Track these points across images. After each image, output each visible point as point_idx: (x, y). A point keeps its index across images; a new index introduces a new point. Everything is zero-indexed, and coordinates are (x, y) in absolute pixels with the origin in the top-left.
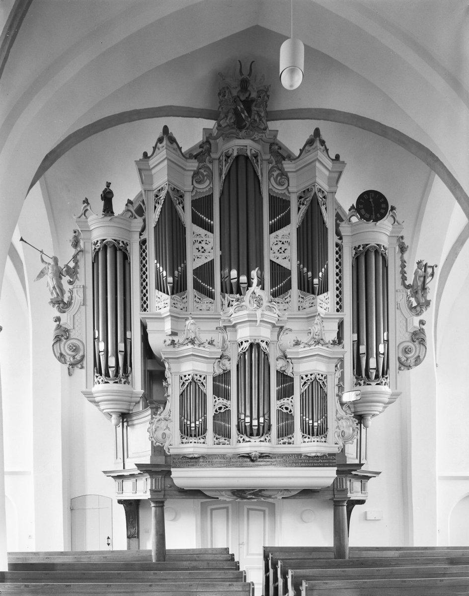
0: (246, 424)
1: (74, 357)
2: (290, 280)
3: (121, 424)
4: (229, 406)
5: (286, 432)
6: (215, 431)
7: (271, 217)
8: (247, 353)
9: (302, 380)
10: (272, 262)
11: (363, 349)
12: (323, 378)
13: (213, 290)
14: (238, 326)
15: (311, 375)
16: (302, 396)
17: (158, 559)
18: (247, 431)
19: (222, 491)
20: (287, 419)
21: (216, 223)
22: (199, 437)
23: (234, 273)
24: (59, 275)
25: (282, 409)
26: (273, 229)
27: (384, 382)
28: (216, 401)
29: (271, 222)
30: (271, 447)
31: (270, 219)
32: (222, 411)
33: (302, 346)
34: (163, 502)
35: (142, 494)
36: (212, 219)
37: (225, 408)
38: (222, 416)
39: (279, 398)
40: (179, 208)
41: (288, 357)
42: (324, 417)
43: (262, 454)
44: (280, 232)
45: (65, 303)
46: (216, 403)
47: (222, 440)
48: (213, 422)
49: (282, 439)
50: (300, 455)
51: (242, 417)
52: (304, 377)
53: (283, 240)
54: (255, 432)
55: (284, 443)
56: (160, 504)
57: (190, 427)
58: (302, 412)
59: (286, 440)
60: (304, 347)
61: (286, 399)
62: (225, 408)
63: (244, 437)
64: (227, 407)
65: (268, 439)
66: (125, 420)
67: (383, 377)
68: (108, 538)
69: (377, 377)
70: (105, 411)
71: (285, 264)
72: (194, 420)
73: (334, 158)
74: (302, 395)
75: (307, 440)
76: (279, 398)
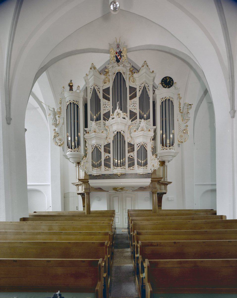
1: (60, 143)
3: (78, 166)
6: (105, 165)
7: (130, 93)
8: (116, 136)
10: (130, 111)
11: (164, 136)
14: (113, 125)
15: (141, 143)
17: (87, 214)
18: (116, 165)
20: (132, 161)
21: (111, 97)
24: (55, 114)
30: (125, 171)
31: (130, 94)
32: (107, 158)
34: (89, 193)
35: (81, 191)
36: (109, 95)
38: (107, 160)
39: (129, 153)
40: (98, 92)
44: (133, 100)
45: (57, 124)
47: (107, 168)
51: (115, 160)
52: (138, 144)
54: (119, 165)
55: (131, 170)
56: (88, 194)
57: (95, 164)
58: (138, 157)
59: (131, 168)
60: (138, 132)
61: (131, 153)
63: (115, 167)
64: (109, 156)
65: (124, 168)
66: (79, 165)
67: (172, 146)
68: (77, 207)
70: (72, 161)
71: (135, 111)
73: (152, 72)
74: (138, 151)
75: (139, 168)
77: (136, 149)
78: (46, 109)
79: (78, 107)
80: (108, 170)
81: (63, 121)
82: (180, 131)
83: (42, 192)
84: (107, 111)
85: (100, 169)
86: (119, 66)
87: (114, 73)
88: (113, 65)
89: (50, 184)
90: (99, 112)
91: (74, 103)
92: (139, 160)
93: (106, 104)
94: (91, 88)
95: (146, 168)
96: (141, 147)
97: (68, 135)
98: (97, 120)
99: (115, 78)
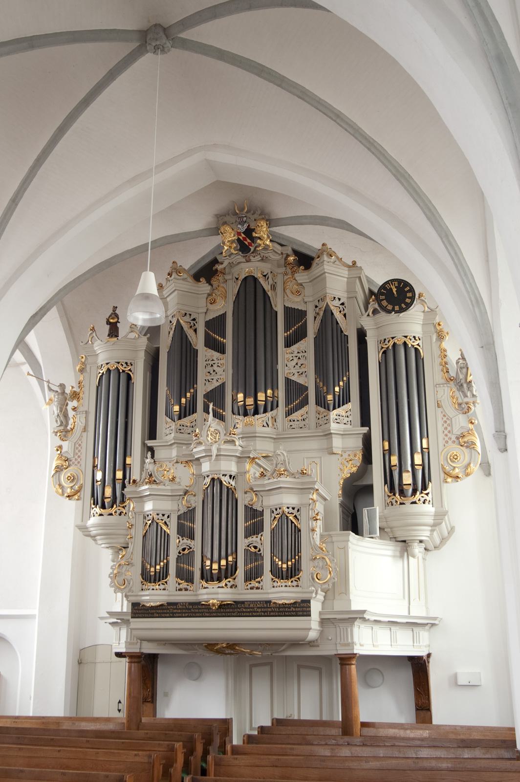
0: (151, 573)
2: (307, 396)
4: (193, 547)
5: (253, 574)
9: (272, 514)
10: (288, 381)
11: (395, 460)
12: (295, 512)
13: (224, 413)
16: (272, 532)
18: (207, 576)
19: (195, 644)
20: (256, 560)
21: (229, 342)
22: (159, 583)
23: (240, 396)
25: (250, 549)
26: (289, 343)
27: (422, 500)
28: (179, 542)
29: (286, 334)
32: (186, 552)
33: (266, 478)
36: (224, 338)
37: (188, 549)
38: (185, 557)
39: (246, 537)
40: (190, 333)
41: (254, 490)
42: (297, 557)
43: (222, 602)
44: (295, 348)
45: (67, 431)
46: (180, 544)
47: (184, 584)
48: (177, 565)
49: (250, 584)
50: (270, 602)
53: (299, 355)
55: (252, 588)
60: (269, 479)
61: (254, 537)
62: (188, 549)
64: (191, 548)
65: (229, 585)
69: (414, 492)
71: (301, 380)
72: (154, 565)
74: (273, 531)
76: (246, 537)
77: (268, 525)
78: (42, 367)
79: (129, 378)
80: (186, 590)
81: (84, 421)
82: (450, 439)
83: (9, 642)
84: (216, 384)
85: (162, 587)
86: (248, 261)
87: (237, 279)
88: (233, 260)
89: (36, 612)
90: (192, 391)
91: (119, 370)
92: (277, 560)
93: (214, 362)
94: (171, 322)
95: (295, 583)
96: (280, 520)
97: (96, 463)
98: (182, 416)
99: (238, 292)
